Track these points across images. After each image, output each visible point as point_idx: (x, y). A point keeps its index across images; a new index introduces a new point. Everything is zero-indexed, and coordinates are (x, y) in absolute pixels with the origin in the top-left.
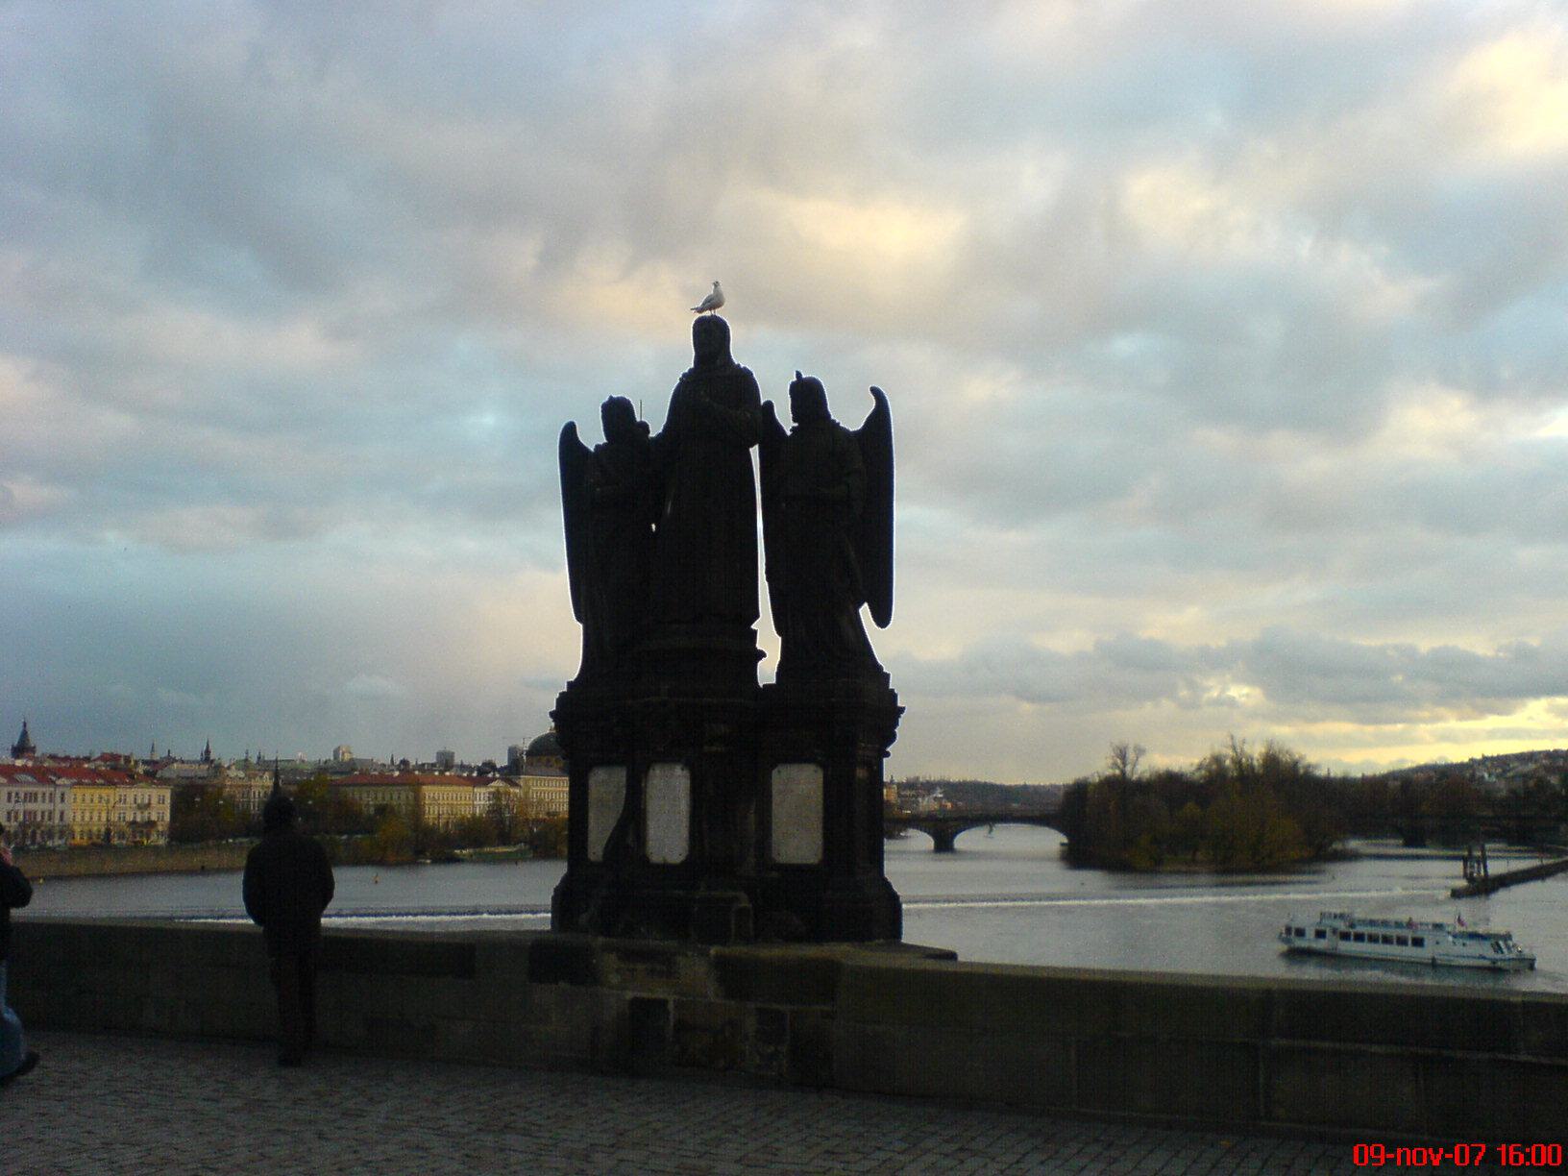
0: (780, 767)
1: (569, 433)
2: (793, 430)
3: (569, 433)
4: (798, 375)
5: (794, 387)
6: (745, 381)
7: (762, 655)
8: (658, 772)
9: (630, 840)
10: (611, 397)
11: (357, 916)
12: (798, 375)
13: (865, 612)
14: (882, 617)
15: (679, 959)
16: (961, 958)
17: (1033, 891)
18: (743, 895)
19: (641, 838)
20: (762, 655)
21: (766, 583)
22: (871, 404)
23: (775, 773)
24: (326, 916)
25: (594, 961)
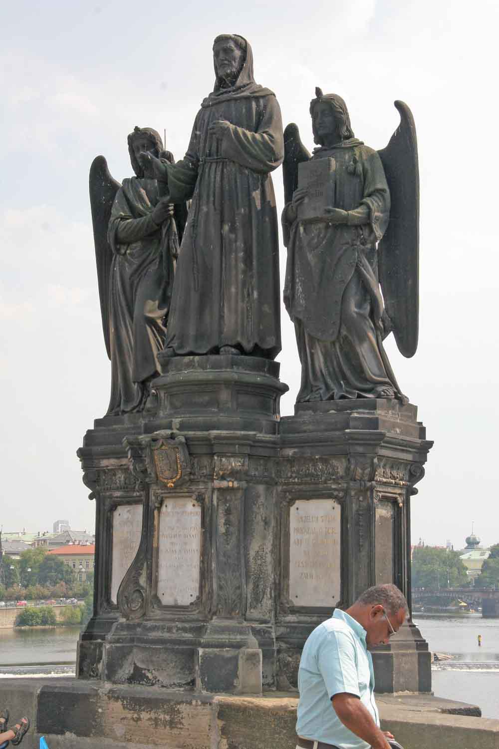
0: (298, 503)
1: (99, 167)
2: (316, 151)
3: (99, 167)
4: (318, 91)
5: (314, 104)
6: (265, 98)
7: (285, 388)
8: (169, 509)
9: (143, 581)
10: (137, 129)
11: (8, 673)
12: (318, 91)
13: (390, 343)
14: (408, 347)
15: (182, 707)
16: (361, 700)
17: (138, 293)
18: (253, 640)
19: (153, 580)
20: (285, 388)
21: (284, 304)
22: (395, 120)
23: (293, 510)
24: (328, 708)
25: (100, 710)
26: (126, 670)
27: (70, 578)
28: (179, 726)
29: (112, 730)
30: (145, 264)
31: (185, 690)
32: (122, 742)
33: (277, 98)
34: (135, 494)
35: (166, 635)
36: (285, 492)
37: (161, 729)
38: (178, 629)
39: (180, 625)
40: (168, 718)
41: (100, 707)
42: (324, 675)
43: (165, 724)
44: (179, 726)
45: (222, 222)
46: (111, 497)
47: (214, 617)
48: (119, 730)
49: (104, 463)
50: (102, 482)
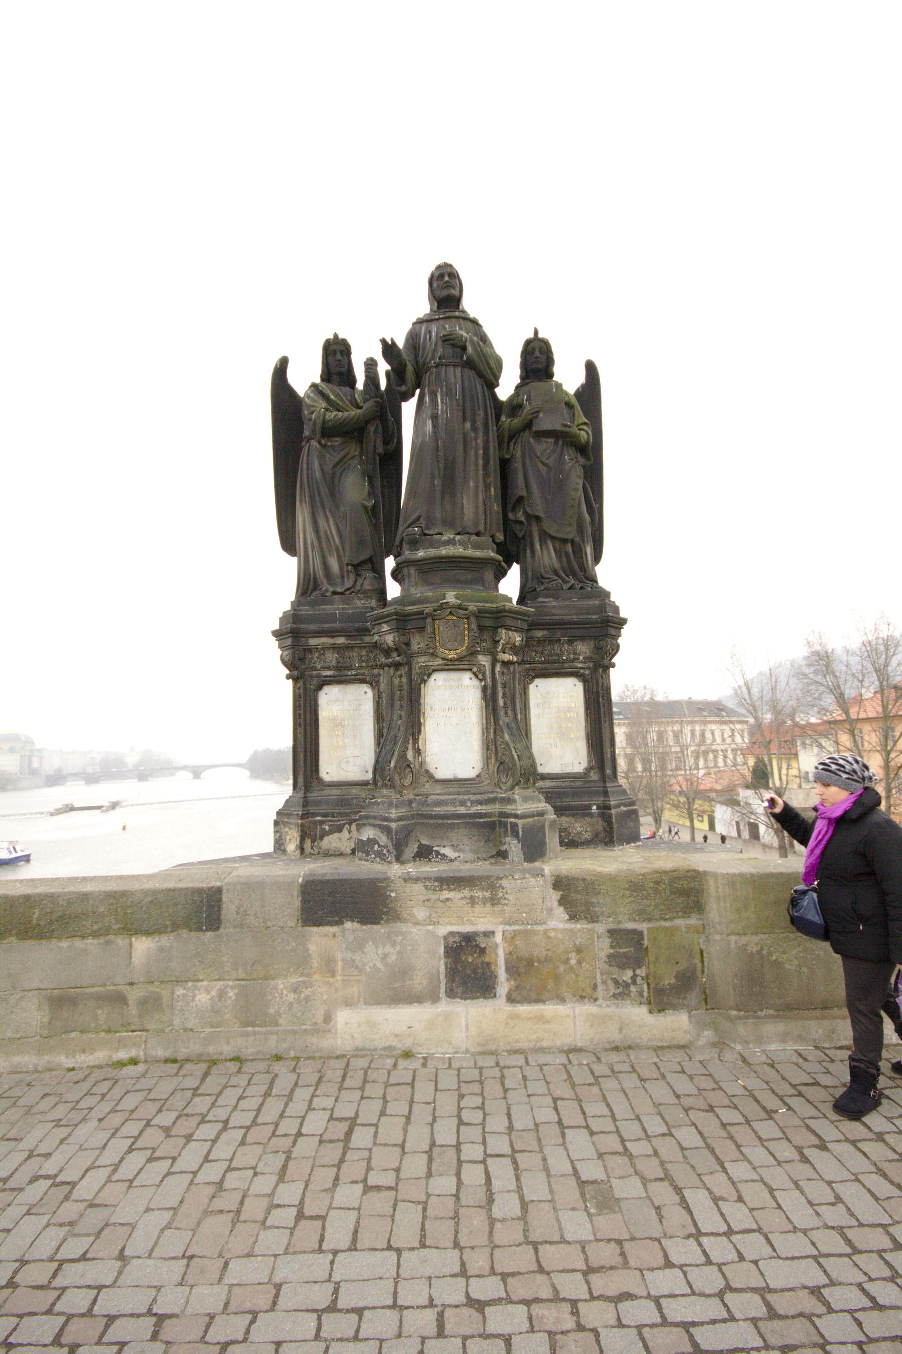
0: (537, 681)
4: (536, 332)
5: (528, 343)
12: (536, 332)
25: (393, 895)
26: (413, 848)
27: (692, 752)
28: (504, 902)
29: (412, 915)
30: (346, 459)
31: (491, 864)
32: (426, 925)
33: (484, 328)
34: (350, 674)
35: (462, 810)
36: (529, 670)
37: (478, 908)
38: (472, 802)
39: (472, 797)
40: (487, 895)
41: (392, 891)
42: (112, 812)
43: (484, 901)
44: (504, 902)
45: (464, 419)
46: (319, 676)
47: (517, 788)
48: (421, 913)
49: (313, 642)
50: (307, 662)
